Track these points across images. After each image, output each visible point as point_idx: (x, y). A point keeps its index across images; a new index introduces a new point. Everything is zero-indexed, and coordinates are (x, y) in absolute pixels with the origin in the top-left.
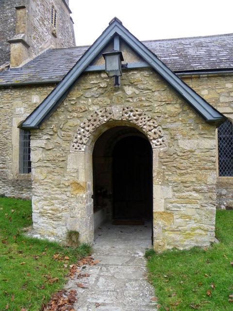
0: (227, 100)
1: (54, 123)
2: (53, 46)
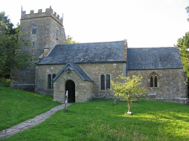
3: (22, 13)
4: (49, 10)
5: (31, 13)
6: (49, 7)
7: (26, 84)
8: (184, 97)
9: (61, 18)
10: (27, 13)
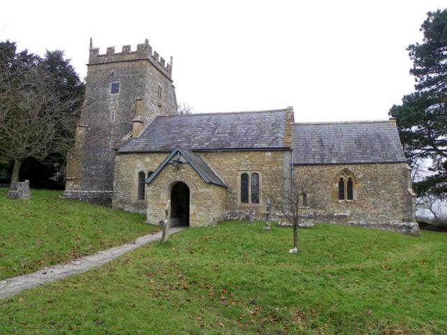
1: (156, 181)
2: (159, 114)
4: (145, 48)
5: (108, 53)
6: (143, 42)
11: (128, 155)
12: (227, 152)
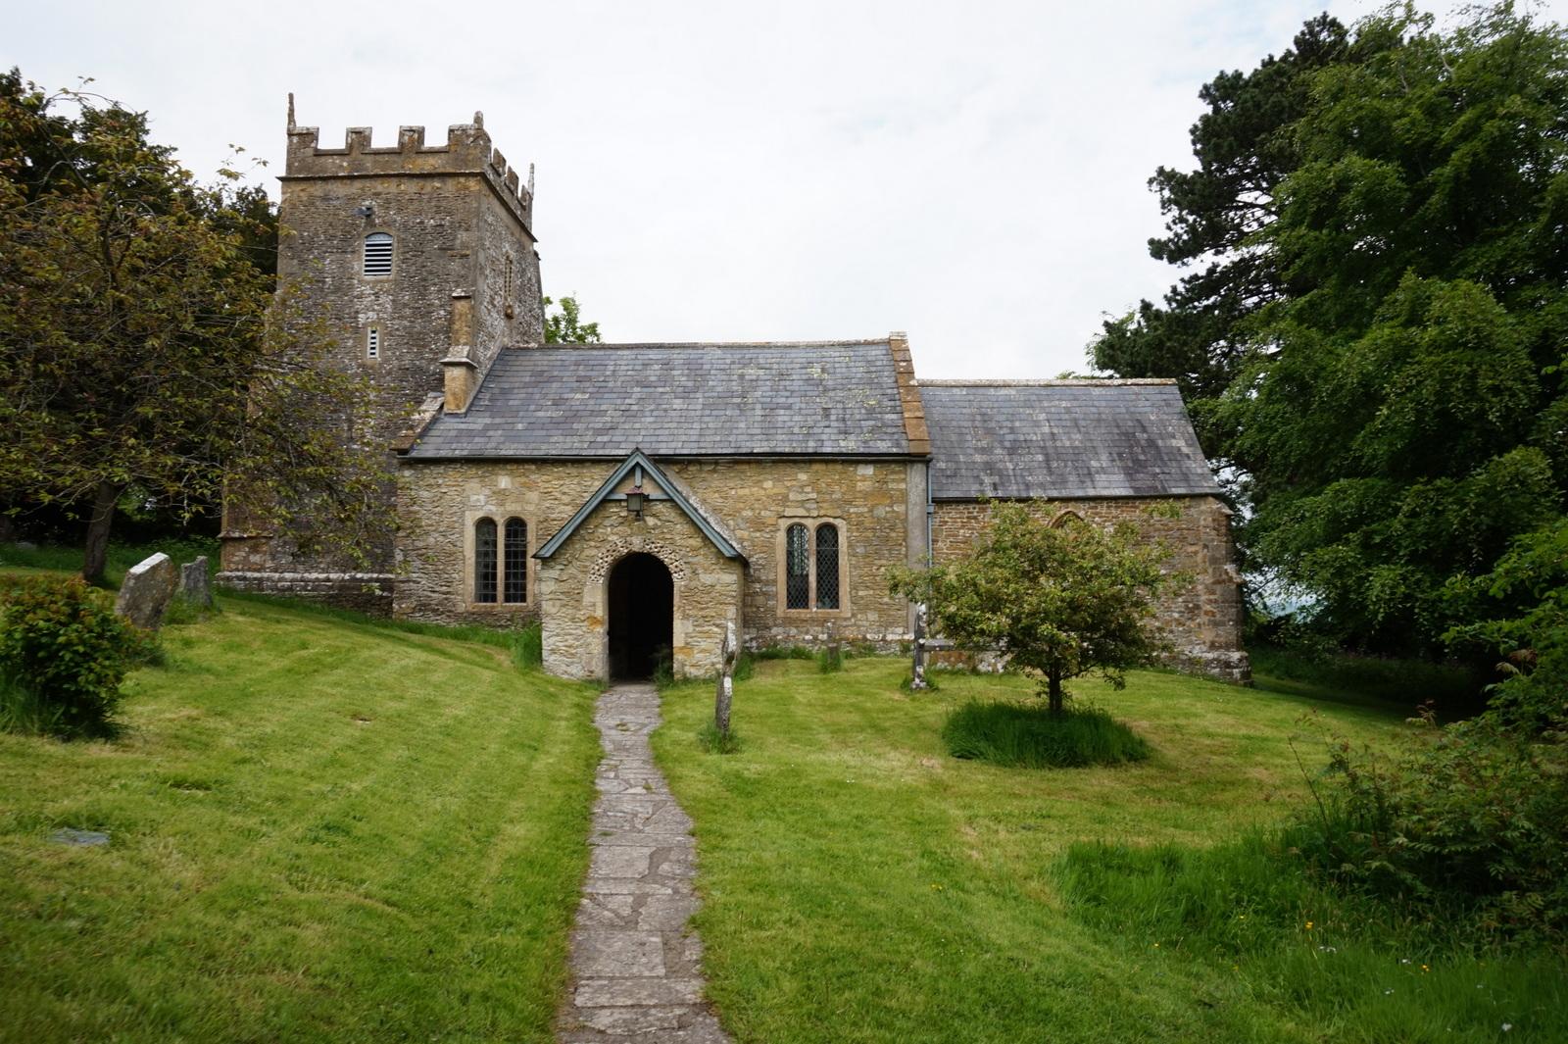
0: (800, 497)
3: (291, 142)
4: (470, 140)
5: (350, 147)
6: (469, 121)
7: (324, 571)
8: (1227, 647)
9: (525, 193)
10: (324, 143)
11: (441, 469)
12: (749, 462)
